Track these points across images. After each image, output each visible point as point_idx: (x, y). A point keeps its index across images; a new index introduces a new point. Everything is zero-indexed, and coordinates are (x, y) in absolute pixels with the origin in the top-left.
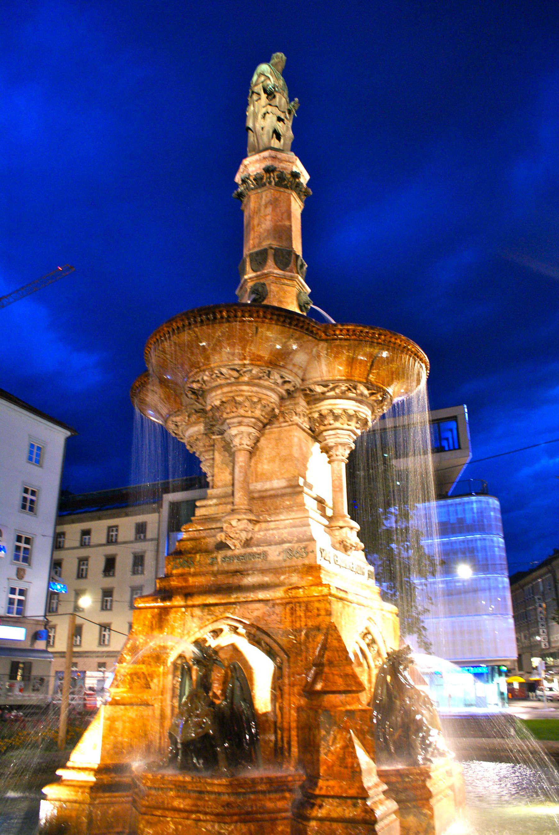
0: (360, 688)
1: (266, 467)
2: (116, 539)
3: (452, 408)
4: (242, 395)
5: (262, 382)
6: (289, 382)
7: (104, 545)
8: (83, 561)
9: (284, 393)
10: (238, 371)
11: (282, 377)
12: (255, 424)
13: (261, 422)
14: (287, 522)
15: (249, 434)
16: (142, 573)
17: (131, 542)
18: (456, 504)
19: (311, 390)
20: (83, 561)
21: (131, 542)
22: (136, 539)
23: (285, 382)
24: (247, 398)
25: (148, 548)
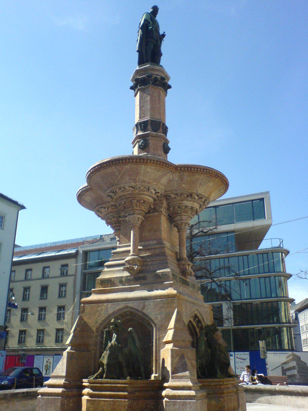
0: (222, 325)
1: (146, 234)
2: (67, 273)
3: (166, 105)
4: (135, 199)
5: (145, 192)
6: (159, 192)
7: (40, 279)
8: (26, 289)
9: (156, 197)
10: (133, 188)
11: (155, 190)
12: (141, 213)
13: (144, 212)
14: (157, 262)
15: (142, 219)
16: (46, 298)
17: (58, 277)
18: (219, 258)
19: (169, 196)
20: (26, 289)
21: (58, 277)
22: (61, 275)
23: (156, 193)
24: (137, 201)
25: (69, 280)
